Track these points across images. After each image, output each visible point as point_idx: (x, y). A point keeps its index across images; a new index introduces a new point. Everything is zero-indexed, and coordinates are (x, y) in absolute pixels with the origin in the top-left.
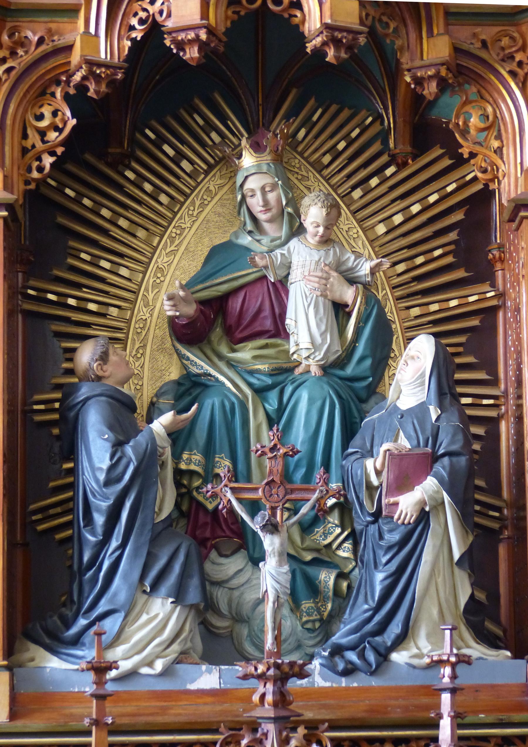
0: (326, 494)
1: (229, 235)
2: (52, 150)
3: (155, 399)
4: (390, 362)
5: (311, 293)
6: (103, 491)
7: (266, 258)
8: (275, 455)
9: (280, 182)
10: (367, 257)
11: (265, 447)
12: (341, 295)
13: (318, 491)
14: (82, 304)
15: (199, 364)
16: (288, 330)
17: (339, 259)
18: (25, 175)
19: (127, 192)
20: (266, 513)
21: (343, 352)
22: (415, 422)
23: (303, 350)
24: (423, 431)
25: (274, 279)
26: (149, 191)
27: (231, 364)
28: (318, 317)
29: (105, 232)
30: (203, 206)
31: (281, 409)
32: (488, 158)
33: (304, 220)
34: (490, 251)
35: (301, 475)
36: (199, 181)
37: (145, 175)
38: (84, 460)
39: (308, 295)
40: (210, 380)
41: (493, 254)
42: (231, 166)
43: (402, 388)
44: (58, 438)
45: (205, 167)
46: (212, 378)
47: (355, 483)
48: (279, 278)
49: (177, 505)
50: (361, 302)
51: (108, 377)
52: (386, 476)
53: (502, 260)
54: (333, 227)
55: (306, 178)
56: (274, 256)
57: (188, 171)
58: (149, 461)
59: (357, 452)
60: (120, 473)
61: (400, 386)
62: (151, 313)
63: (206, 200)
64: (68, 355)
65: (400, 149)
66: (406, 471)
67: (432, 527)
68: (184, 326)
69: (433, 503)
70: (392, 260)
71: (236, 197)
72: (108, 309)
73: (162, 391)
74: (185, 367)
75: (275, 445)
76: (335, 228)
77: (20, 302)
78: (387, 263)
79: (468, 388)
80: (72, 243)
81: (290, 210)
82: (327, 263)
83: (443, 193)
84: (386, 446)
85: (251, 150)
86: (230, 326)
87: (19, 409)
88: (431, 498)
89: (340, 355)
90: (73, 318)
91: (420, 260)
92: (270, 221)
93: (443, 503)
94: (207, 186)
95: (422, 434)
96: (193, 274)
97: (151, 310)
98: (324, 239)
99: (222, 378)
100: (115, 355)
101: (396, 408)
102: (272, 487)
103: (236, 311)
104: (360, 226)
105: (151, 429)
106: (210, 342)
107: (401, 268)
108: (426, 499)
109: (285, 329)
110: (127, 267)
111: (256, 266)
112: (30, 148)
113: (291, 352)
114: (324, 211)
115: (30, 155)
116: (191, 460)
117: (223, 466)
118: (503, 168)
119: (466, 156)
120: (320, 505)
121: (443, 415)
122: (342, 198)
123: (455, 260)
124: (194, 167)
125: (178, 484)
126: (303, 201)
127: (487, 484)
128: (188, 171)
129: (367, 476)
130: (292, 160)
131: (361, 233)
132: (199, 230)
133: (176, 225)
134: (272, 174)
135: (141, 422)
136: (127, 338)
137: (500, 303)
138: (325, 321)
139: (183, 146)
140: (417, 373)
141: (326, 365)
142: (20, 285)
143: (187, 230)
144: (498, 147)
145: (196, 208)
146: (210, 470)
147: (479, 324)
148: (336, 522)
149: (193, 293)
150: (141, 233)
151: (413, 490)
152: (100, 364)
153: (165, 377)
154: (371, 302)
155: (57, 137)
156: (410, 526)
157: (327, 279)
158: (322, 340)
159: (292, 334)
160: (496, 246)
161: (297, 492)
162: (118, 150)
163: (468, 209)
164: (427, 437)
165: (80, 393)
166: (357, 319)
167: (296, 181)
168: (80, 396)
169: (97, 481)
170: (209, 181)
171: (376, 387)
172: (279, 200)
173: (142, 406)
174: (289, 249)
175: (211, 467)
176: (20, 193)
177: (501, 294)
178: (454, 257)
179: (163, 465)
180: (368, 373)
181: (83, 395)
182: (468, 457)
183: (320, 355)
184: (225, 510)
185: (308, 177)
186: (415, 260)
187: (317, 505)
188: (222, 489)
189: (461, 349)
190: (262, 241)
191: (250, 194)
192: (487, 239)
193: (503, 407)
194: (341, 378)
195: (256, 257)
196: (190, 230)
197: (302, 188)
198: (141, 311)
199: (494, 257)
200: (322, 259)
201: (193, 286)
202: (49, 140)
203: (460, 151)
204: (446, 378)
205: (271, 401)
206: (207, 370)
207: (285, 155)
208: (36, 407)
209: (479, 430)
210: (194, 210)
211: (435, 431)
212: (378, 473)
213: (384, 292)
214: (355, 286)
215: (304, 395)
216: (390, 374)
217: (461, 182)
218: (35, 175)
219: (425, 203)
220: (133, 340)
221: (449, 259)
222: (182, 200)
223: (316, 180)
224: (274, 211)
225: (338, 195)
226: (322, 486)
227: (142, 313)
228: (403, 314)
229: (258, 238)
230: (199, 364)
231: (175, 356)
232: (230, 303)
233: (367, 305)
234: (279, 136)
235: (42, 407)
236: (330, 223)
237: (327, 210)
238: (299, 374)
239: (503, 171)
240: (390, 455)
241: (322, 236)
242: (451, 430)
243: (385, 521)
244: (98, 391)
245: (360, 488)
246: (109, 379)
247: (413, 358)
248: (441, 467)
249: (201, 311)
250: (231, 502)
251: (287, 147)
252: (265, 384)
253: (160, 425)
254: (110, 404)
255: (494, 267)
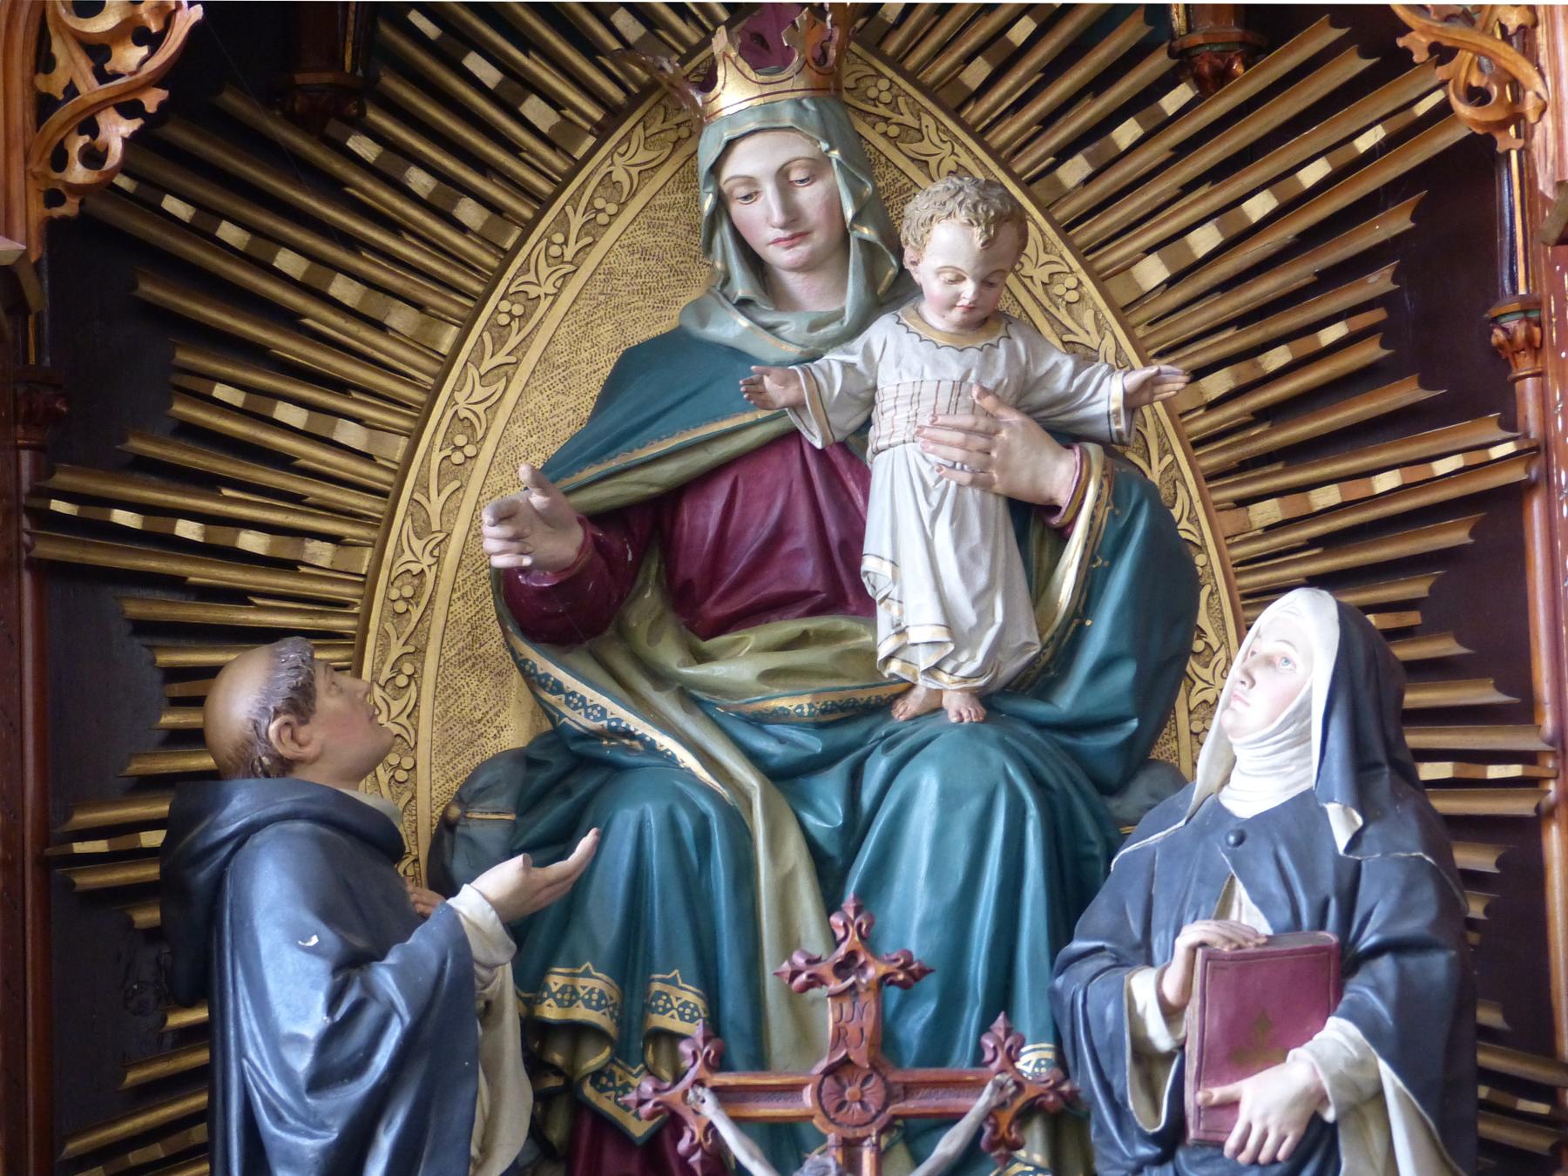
0: (1015, 1095)
1: (676, 312)
2: (130, 98)
3: (455, 812)
4: (1193, 666)
5: (941, 478)
6: (305, 1105)
7: (797, 379)
8: (853, 986)
9: (835, 154)
10: (1111, 360)
11: (818, 960)
12: (1034, 480)
13: (989, 1087)
14: (221, 536)
15: (592, 703)
16: (870, 590)
17: (1026, 372)
18: (46, 176)
19: (353, 197)
20: (831, 1162)
21: (1045, 647)
22: (1284, 855)
23: (921, 648)
24: (1309, 882)
25: (824, 438)
26: (423, 194)
27: (691, 697)
28: (966, 548)
29: (289, 320)
30: (594, 229)
31: (855, 827)
32: (1490, 59)
33: (914, 263)
34: (1495, 320)
35: (923, 1021)
36: (578, 155)
37: (411, 147)
38: (242, 1013)
39: (931, 483)
40: (629, 749)
41: (1505, 330)
42: (680, 109)
43: (1237, 751)
44: (153, 935)
45: (596, 114)
46: (636, 743)
47: (1096, 1043)
48: (839, 437)
49: (537, 1131)
50: (1098, 497)
51: (315, 759)
52: (1196, 1022)
53: (1534, 347)
54: (1004, 277)
55: (912, 132)
56: (823, 372)
57: (544, 127)
58: (449, 1008)
59: (1101, 949)
60: (358, 1051)
61: (1230, 745)
62: (436, 553)
63: (603, 210)
64: (178, 690)
65: (1205, 34)
66: (1259, 1007)
67: (1348, 1169)
68: (543, 593)
69: (1350, 1098)
70: (1189, 363)
71: (697, 201)
72: (302, 549)
73: (478, 784)
74: (548, 711)
75: (852, 955)
76: (1011, 279)
77: (26, 538)
78: (1175, 380)
79: (1441, 732)
80: (185, 357)
81: (867, 232)
82: (989, 384)
83: (1343, 156)
84: (1192, 933)
85: (741, 63)
86: (688, 584)
87: (29, 854)
88: (1340, 1081)
89: (1037, 657)
90: (192, 579)
91: (1277, 358)
92: (806, 267)
93: (1379, 1094)
94: (604, 170)
95: (1305, 890)
96: (565, 434)
97: (438, 545)
98: (979, 314)
99: (666, 742)
100: (334, 692)
101: (1220, 813)
102: (845, 1081)
103: (704, 537)
104: (1087, 267)
105: (454, 916)
106: (623, 634)
107: (1219, 383)
108: (1327, 1086)
109: (860, 588)
110: (358, 420)
111: (765, 404)
112: (61, 97)
113: (883, 653)
114: (977, 236)
115: (60, 116)
116: (574, 992)
117: (678, 1007)
118: (1539, 88)
119: (1420, 56)
120: (996, 1128)
121: (1370, 830)
122: (1027, 185)
123: (1385, 352)
124: (563, 116)
125: (535, 1065)
126: (909, 208)
127: (1507, 1018)
128: (545, 129)
129: (1137, 1022)
130: (869, 82)
131: (1089, 286)
132: (581, 303)
133: (511, 290)
134: (808, 128)
135: (420, 895)
136: (365, 630)
137: (1534, 473)
138: (985, 559)
139: (528, 56)
140: (1285, 707)
141: (994, 688)
142: (25, 487)
143: (544, 304)
144: (1521, 27)
145: (572, 238)
146: (635, 1019)
147: (1470, 541)
148: (1038, 1158)
149: (568, 493)
150: (401, 318)
151: (1284, 1059)
152: (287, 724)
153: (483, 740)
154: (1130, 497)
155: (144, 60)
156: (1277, 1169)
157: (990, 434)
158: (980, 616)
159: (882, 601)
160: (1516, 306)
161: (923, 1092)
162: (327, 78)
163: (1423, 200)
164: (1321, 897)
165: (228, 812)
166: (1086, 546)
167: (882, 144)
168: (228, 823)
169: (286, 1074)
170: (611, 154)
171: (1152, 743)
172: (834, 206)
173: (416, 832)
174: (867, 350)
175: (637, 1009)
176: (33, 232)
177: (1537, 448)
178: (1383, 345)
179: (489, 1012)
180: (1125, 707)
181: (236, 816)
182: (1453, 953)
183: (972, 662)
184: (697, 1156)
185: (920, 130)
186: (1260, 358)
187: (988, 1130)
188: (686, 1093)
189: (1413, 618)
190: (782, 328)
191: (742, 191)
192: (1488, 286)
193: (1552, 786)
194: (1040, 726)
195: (766, 379)
196: (553, 303)
197: (902, 162)
198: (406, 548)
199: (1511, 338)
200: (973, 374)
201: (569, 472)
202: (120, 69)
203: (1401, 42)
204: (1372, 714)
205: (821, 804)
206: (619, 720)
207: (846, 68)
208: (79, 848)
209: (1477, 858)
210: (566, 242)
211: (1347, 878)
212: (1171, 1013)
213: (1168, 459)
214: (1077, 450)
215: (927, 783)
216: (1195, 700)
217: (1400, 121)
218: (78, 173)
219: (1289, 190)
220: (384, 635)
221: (1371, 351)
222: (527, 213)
223: (945, 138)
224: (818, 238)
225: (1015, 178)
226: (1001, 1071)
227: (408, 556)
228: (1229, 521)
229: (769, 319)
230: (592, 703)
231: (516, 678)
232: (685, 515)
233: (1116, 505)
234: (829, 17)
235: (101, 846)
236: (993, 268)
237: (987, 231)
238: (908, 720)
239: (1538, 95)
240: (1208, 958)
241: (970, 309)
242: (1398, 876)
243: (1197, 1157)
244: (284, 804)
245: (1112, 1061)
246: (318, 765)
247: (1269, 661)
248: (1371, 988)
249: (599, 545)
250: (716, 1133)
251: (853, 46)
252: (798, 754)
253: (481, 898)
254: (322, 842)
255: (1509, 369)
